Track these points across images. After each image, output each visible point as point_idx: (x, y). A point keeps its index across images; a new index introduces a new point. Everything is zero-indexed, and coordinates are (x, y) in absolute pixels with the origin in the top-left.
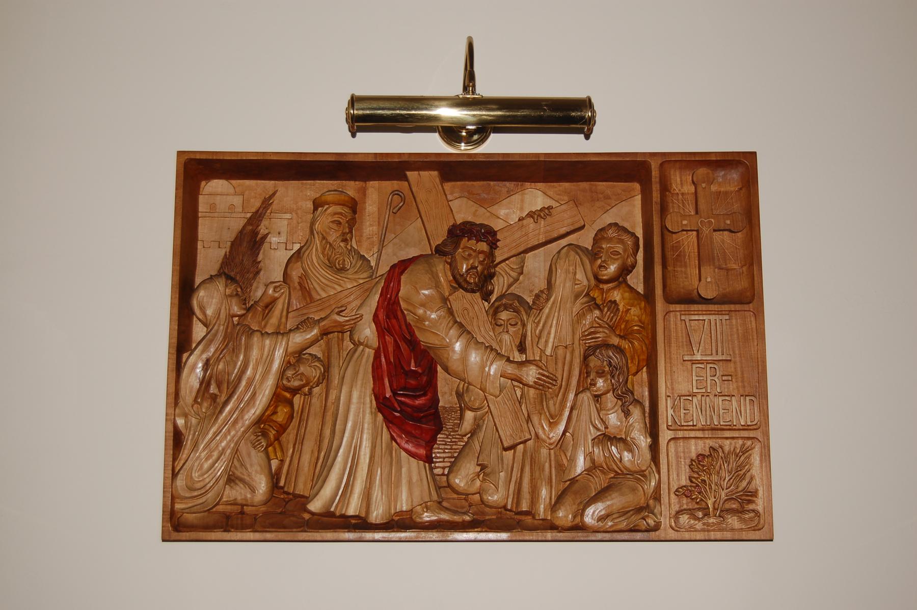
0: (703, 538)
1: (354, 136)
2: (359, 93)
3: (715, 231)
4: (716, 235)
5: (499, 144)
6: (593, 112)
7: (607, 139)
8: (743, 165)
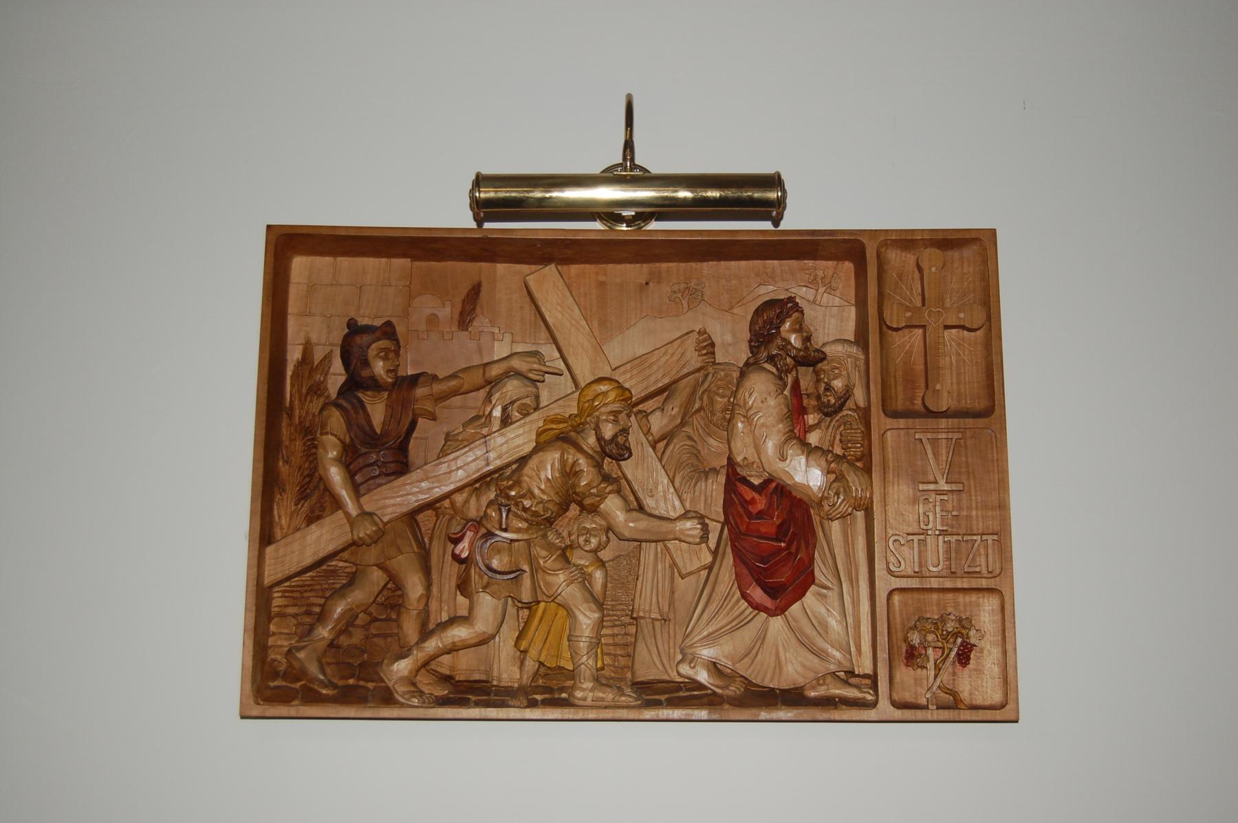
2: (487, 171)
7: (795, 219)
8: (978, 244)
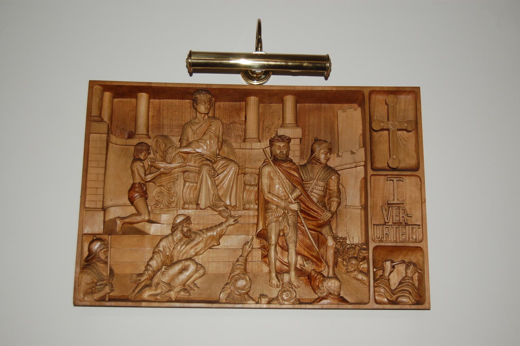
0: (320, 307)
1: (191, 75)
2: (194, 50)
3: (398, 130)
4: (399, 133)
5: (276, 81)
6: (330, 64)
7: (339, 78)
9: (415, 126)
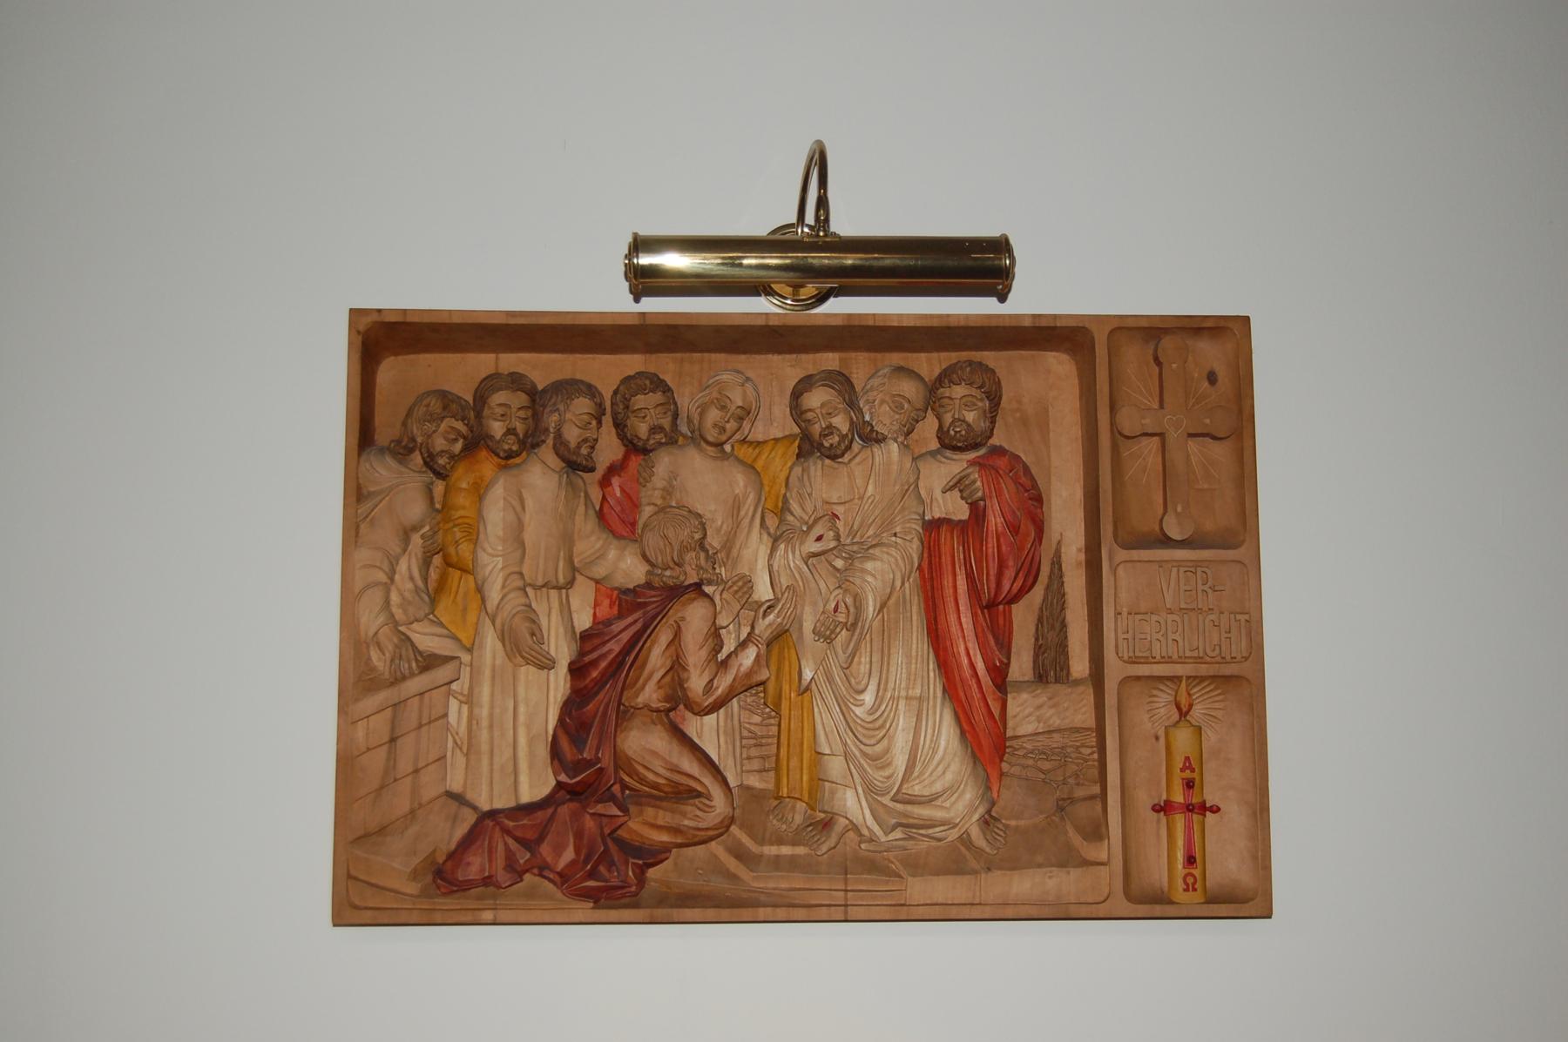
1: (637, 300)
2: (645, 231)
5: (840, 307)
7: (1029, 298)
9: (1234, 425)
